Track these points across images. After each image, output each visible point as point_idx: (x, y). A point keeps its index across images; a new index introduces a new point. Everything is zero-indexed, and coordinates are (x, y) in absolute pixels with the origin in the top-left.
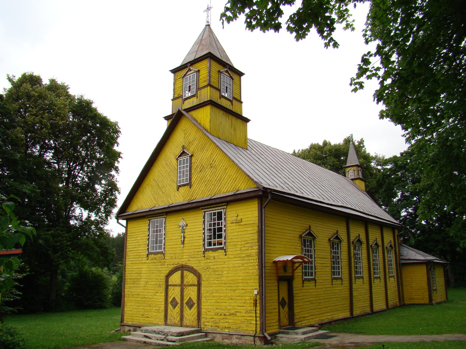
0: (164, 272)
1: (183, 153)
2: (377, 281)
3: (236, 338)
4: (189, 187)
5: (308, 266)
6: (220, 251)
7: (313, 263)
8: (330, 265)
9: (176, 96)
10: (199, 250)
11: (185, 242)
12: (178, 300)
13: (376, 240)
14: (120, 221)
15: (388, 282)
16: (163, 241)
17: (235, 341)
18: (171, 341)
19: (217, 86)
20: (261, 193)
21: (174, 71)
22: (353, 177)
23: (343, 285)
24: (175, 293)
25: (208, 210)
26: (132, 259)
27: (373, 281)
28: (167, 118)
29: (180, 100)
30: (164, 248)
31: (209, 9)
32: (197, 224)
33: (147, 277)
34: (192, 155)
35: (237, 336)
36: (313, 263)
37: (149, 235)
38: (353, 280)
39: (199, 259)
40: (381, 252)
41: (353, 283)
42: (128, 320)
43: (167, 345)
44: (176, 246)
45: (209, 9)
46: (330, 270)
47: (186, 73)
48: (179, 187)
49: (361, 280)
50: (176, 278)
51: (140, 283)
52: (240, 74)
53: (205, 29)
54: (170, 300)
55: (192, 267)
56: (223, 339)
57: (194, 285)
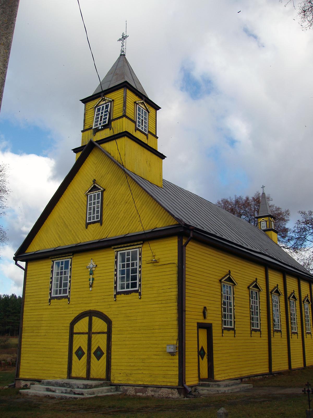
0: (68, 318)
1: (94, 188)
2: (294, 336)
3: (152, 391)
4: (99, 224)
5: (228, 315)
6: (134, 294)
7: (233, 312)
8: (249, 315)
9: (87, 127)
10: (110, 293)
11: (94, 285)
12: (85, 350)
13: (294, 293)
14: (19, 262)
15: (305, 339)
16: (69, 284)
17: (150, 393)
18: (78, 394)
19: (133, 118)
20: (182, 230)
21: (85, 101)
22: (265, 228)
23: (262, 338)
24: (81, 342)
25: (121, 249)
26: (31, 305)
27: (290, 337)
28: (76, 151)
29: (91, 132)
30: (69, 292)
31: (124, 38)
32: (106, 264)
33: (49, 325)
34: (104, 190)
35: (152, 388)
36: (233, 312)
37: (52, 278)
38: (272, 334)
39: (110, 303)
40: (299, 306)
41: (272, 336)
42: (22, 375)
43: (75, 398)
44: (82, 289)
45: (124, 38)
46: (249, 321)
47: (99, 103)
48: (87, 224)
49: (279, 334)
50: (82, 325)
51: (40, 331)
52: (157, 108)
53: (119, 59)
54: (75, 349)
55: (102, 313)
56: (136, 392)
57: (103, 333)
